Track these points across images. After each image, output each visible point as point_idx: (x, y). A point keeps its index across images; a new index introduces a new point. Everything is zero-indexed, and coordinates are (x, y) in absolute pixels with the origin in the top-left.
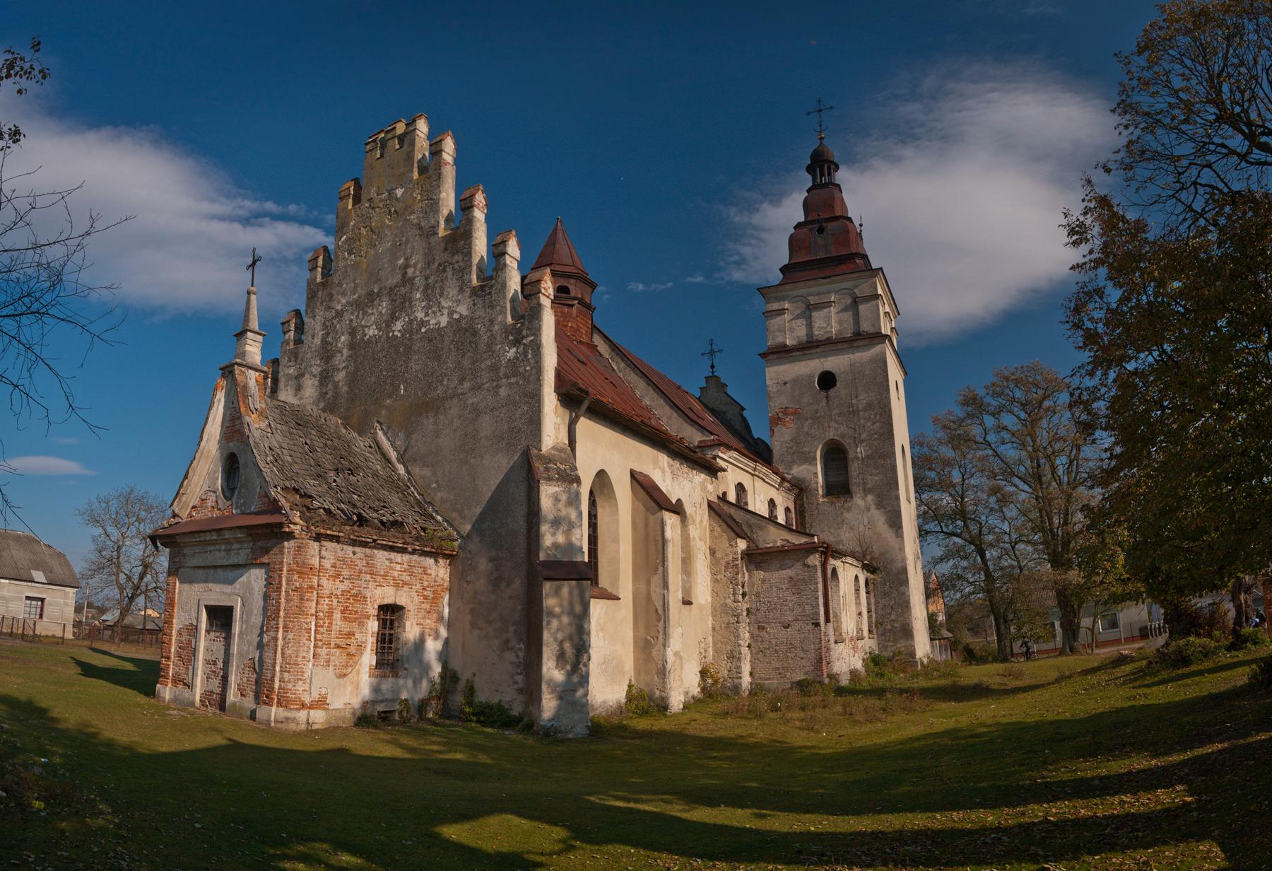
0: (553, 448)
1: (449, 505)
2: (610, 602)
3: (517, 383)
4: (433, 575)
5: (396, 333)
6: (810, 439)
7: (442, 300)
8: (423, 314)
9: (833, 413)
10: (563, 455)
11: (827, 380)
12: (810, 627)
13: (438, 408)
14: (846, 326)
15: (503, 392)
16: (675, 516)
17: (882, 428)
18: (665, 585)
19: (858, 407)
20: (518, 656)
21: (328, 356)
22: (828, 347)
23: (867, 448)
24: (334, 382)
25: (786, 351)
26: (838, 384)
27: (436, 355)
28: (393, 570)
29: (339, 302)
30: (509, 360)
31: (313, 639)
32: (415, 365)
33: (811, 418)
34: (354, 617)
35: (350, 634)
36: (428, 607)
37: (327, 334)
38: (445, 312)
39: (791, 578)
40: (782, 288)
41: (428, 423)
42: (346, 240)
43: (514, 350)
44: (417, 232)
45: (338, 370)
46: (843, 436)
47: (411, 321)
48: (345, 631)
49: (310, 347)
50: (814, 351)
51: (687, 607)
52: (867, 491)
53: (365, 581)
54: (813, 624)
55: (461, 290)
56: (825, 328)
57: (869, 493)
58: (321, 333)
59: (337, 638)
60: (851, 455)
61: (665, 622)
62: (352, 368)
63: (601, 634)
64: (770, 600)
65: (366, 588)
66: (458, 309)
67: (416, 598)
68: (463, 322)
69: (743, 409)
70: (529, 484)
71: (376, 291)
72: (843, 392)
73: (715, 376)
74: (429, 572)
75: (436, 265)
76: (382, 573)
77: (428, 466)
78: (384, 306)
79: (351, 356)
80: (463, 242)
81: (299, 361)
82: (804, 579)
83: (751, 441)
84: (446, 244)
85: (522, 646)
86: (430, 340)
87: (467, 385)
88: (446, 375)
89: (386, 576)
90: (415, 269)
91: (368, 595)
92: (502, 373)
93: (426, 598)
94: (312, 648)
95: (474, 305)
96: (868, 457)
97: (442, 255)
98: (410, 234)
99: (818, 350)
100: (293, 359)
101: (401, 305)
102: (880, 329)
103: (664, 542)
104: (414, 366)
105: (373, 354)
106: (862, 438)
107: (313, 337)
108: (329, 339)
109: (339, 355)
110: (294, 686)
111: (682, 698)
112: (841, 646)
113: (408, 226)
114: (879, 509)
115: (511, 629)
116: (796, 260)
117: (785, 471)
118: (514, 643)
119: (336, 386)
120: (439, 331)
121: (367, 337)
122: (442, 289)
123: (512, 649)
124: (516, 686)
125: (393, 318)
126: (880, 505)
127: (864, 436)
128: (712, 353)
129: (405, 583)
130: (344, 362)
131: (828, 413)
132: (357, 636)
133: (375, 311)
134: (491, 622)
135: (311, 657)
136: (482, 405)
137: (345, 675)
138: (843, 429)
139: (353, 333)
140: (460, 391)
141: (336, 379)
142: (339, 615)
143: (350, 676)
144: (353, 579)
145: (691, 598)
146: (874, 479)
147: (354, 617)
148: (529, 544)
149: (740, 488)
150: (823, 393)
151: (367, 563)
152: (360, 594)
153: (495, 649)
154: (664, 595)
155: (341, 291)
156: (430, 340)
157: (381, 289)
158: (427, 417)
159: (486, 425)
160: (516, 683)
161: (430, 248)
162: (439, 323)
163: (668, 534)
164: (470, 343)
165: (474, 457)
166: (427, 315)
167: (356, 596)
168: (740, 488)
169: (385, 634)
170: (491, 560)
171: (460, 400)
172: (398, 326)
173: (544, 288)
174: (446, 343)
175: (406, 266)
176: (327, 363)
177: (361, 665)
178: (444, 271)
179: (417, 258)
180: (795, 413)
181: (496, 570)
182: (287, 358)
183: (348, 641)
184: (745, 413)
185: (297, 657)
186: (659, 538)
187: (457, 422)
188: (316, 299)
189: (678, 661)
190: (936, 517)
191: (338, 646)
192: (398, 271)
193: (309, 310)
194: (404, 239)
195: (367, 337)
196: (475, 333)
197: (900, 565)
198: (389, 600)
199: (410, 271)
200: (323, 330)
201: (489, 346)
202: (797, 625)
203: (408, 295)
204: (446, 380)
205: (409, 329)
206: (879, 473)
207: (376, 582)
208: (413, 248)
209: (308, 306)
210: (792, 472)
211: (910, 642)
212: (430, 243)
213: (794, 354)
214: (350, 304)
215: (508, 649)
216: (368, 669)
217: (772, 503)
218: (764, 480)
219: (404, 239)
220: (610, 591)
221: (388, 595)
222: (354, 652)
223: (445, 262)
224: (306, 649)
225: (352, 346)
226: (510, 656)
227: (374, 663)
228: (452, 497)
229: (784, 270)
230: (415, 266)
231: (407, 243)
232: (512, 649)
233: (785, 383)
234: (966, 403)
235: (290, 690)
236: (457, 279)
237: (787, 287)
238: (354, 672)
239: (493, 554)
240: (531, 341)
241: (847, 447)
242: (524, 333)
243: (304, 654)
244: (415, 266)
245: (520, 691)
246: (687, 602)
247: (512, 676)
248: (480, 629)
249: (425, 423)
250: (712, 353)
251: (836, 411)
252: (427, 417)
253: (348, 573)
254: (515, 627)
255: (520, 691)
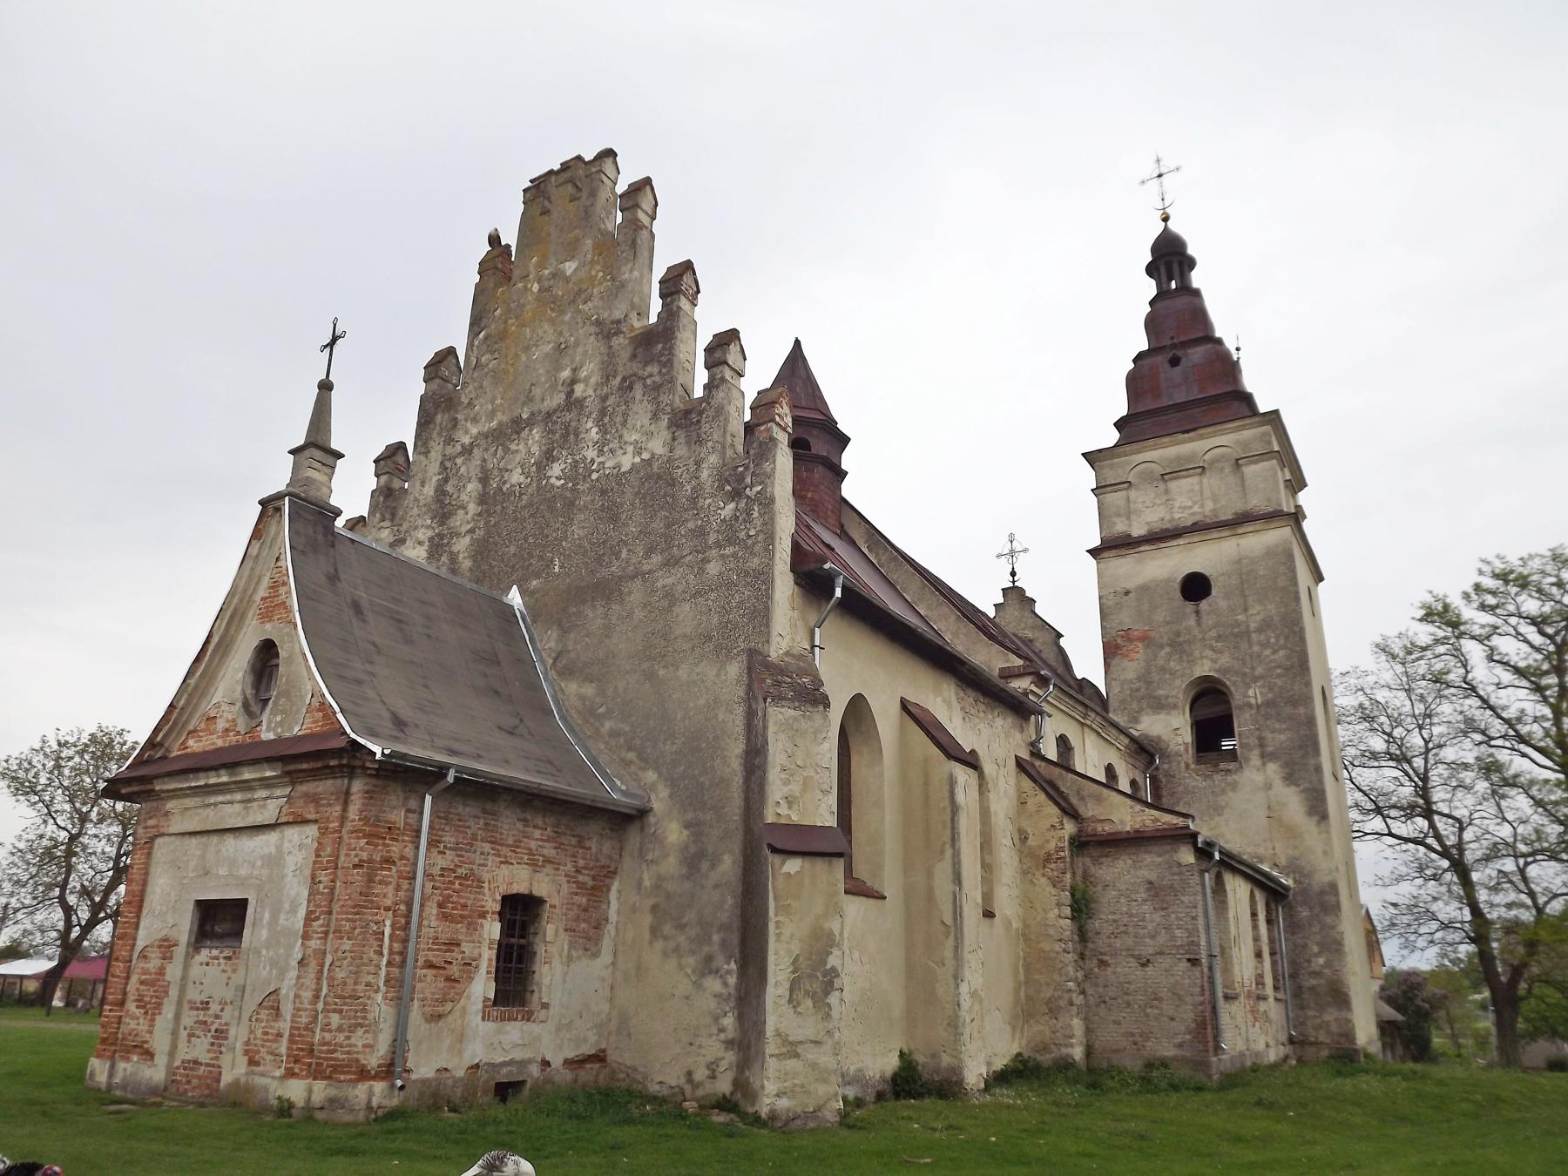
0: (787, 653)
1: (622, 740)
2: (872, 901)
3: (734, 555)
4: (594, 850)
5: (553, 480)
6: (1167, 676)
7: (625, 432)
8: (596, 452)
9: (1207, 636)
10: (801, 664)
11: (1195, 587)
12: (1184, 965)
13: (611, 593)
14: (1224, 503)
15: (713, 568)
16: (970, 771)
17: (1288, 657)
18: (957, 879)
19: (1248, 626)
20: (725, 984)
21: (444, 514)
22: (1196, 537)
23: (1266, 690)
24: (452, 553)
25: (1129, 544)
26: (1214, 592)
27: (612, 515)
28: (528, 837)
29: (467, 432)
30: (724, 521)
31: (386, 952)
32: (579, 528)
33: (1170, 645)
34: (460, 915)
35: (454, 944)
36: (584, 900)
37: (446, 480)
38: (630, 449)
39: (1150, 883)
40: (1121, 450)
41: (594, 616)
42: (486, 338)
43: (732, 505)
44: (593, 329)
45: (458, 535)
46: (1226, 671)
47: (576, 463)
48: (444, 937)
49: (416, 500)
50: (1175, 543)
51: (987, 921)
52: (1266, 757)
53: (482, 853)
54: (1189, 960)
55: (655, 417)
56: (1191, 507)
57: (1270, 760)
58: (435, 479)
59: (429, 949)
60: (1237, 699)
61: (956, 938)
62: (479, 533)
63: (856, 955)
64: (1116, 917)
65: (483, 865)
66: (650, 445)
67: (565, 886)
68: (656, 465)
69: (1060, 635)
70: (750, 707)
71: (525, 416)
72: (1223, 604)
73: (1017, 587)
74: (588, 844)
75: (619, 379)
76: (510, 842)
77: (592, 682)
78: (534, 441)
79: (480, 515)
80: (660, 346)
81: (397, 521)
82: (1171, 886)
83: (1072, 683)
84: (635, 349)
85: (733, 966)
86: (604, 492)
87: (657, 559)
88: (625, 543)
89: (518, 847)
90: (587, 385)
91: (486, 877)
92: (712, 538)
93: (581, 885)
94: (384, 968)
95: (674, 439)
96: (1267, 704)
97: (629, 364)
98: (581, 331)
99: (1181, 541)
100: (388, 516)
101: (562, 435)
102: (1280, 505)
103: (955, 809)
104: (577, 531)
105: (514, 511)
106: (1257, 673)
107: (423, 483)
108: (449, 488)
109: (461, 512)
110: (348, 1038)
111: (984, 1071)
112: (1234, 1007)
113: (579, 320)
114: (1288, 785)
115: (716, 938)
116: (1148, 404)
117: (1130, 725)
118: (719, 961)
119: (453, 558)
120: (619, 477)
121: (508, 486)
122: (625, 415)
123: (717, 971)
124: (722, 1036)
125: (549, 457)
126: (1290, 779)
127: (1260, 670)
128: (1012, 553)
129: (547, 861)
130: (469, 523)
131: (1200, 636)
132: (466, 947)
133: (521, 447)
134: (685, 926)
135: (381, 985)
136: (680, 588)
137: (440, 1016)
138: (1225, 660)
139: (484, 480)
140: (646, 568)
141: (455, 549)
142: (435, 911)
143: (450, 1018)
144: (461, 849)
145: (992, 907)
146: (1278, 738)
147: (460, 915)
148: (747, 800)
149: (1062, 741)
150: (1190, 607)
151: (486, 824)
152: (473, 874)
153: (689, 971)
154: (954, 893)
155: (472, 416)
156: (604, 492)
157: (532, 414)
158: (594, 607)
159: (686, 616)
160: (722, 1030)
161: (611, 354)
162: (619, 466)
163: (960, 797)
164: (666, 495)
165: (664, 667)
166: (601, 452)
167: (466, 878)
168: (1062, 741)
169: (512, 946)
170: (687, 826)
171: (645, 581)
172: (556, 469)
173: (779, 415)
174: (629, 495)
175: (573, 381)
176: (442, 524)
177: (468, 998)
178: (631, 388)
179: (591, 370)
180: (1144, 638)
181: (694, 842)
182: (378, 515)
183: (449, 958)
184: (1062, 642)
185: (356, 983)
186: (947, 803)
187: (639, 614)
188: (431, 426)
189: (977, 1007)
190: (1378, 810)
191: (430, 965)
192: (560, 387)
193: (419, 443)
194: (572, 339)
195: (508, 486)
196: (672, 483)
197: (1327, 879)
198: (520, 888)
199: (579, 389)
200: (439, 474)
201: (694, 500)
202: (1166, 962)
203: (573, 424)
204: (624, 551)
205: (578, 473)
206: (1287, 729)
207: (499, 856)
208: (585, 353)
209: (417, 436)
210: (1139, 727)
211: (1344, 1014)
212: (611, 347)
213: (1142, 548)
214: (486, 436)
215: (710, 973)
216: (480, 1006)
217: (1110, 770)
218: (1098, 734)
219: (572, 339)
220: (869, 884)
221: (519, 880)
222: (457, 975)
223: (631, 376)
224: (372, 969)
225: (483, 499)
226: (713, 985)
227: (492, 996)
228: (627, 729)
229: (1119, 425)
230: (586, 380)
231: (577, 344)
232: (717, 971)
233: (1127, 593)
234: (1429, 616)
235: (341, 1046)
236: (649, 402)
237: (1127, 448)
238: (457, 1013)
239: (690, 816)
240: (758, 493)
241: (1232, 688)
242: (748, 480)
243: (370, 978)
244: (586, 380)
245: (729, 1044)
246: (989, 914)
247: (716, 1019)
248: (666, 938)
249: (591, 615)
250: (1012, 553)
251: (1213, 633)
252: (594, 607)
253: (453, 839)
254: (722, 935)
255: (729, 1044)
